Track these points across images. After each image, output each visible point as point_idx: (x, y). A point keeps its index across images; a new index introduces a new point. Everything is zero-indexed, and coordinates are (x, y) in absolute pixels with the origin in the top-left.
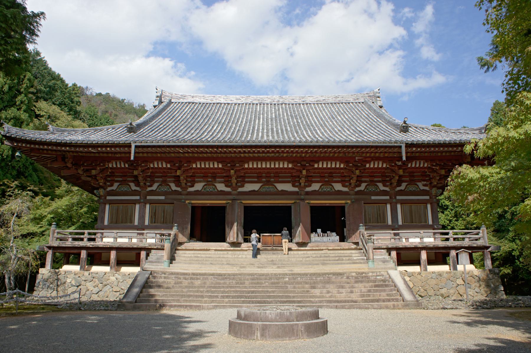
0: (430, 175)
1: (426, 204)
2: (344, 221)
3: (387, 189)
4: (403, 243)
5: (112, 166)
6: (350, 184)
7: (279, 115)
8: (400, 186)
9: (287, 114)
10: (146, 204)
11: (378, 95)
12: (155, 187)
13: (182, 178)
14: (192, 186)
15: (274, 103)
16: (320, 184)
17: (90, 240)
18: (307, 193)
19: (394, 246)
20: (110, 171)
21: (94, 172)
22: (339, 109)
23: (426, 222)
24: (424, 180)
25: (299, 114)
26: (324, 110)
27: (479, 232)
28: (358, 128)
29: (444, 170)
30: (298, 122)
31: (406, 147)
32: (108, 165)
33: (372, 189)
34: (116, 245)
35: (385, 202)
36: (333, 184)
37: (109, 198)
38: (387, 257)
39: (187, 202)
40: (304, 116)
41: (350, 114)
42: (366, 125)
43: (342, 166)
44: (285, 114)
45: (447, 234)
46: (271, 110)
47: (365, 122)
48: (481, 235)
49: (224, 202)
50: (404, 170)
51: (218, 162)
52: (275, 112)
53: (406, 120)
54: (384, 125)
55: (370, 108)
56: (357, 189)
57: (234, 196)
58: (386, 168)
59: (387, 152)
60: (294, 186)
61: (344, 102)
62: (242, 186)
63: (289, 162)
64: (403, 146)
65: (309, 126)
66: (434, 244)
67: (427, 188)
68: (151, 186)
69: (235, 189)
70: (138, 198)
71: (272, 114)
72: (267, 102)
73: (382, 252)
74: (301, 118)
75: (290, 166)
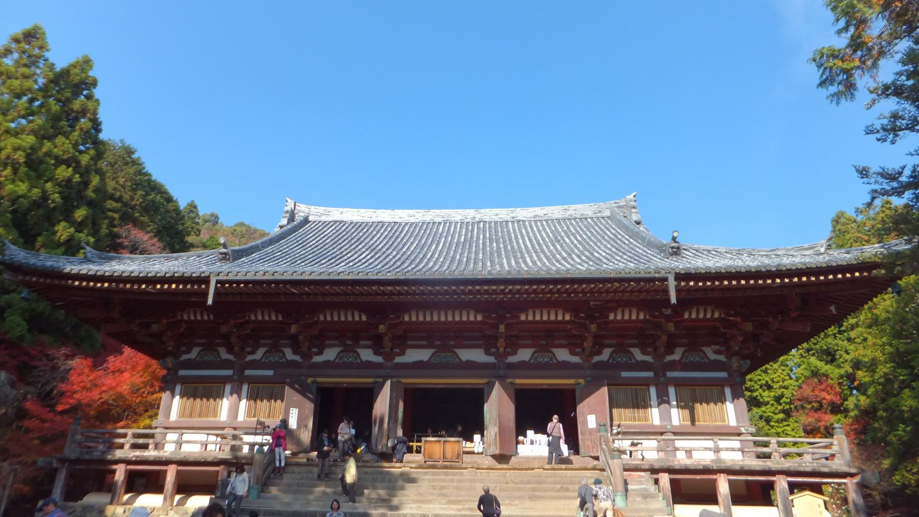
0: (725, 334)
1: (723, 386)
2: (575, 417)
3: (649, 358)
4: (681, 459)
5: (189, 317)
6: (583, 349)
7: (472, 236)
8: (672, 353)
9: (484, 237)
10: (242, 383)
11: (633, 203)
12: (259, 355)
13: (301, 338)
14: (320, 353)
15: (467, 220)
16: (533, 350)
17: (135, 446)
18: (511, 366)
19: (665, 465)
20: (184, 325)
21: (155, 327)
22: (568, 228)
23: (723, 420)
24: (716, 344)
25: (503, 236)
26: (544, 230)
27: (832, 444)
28: (596, 254)
29: (750, 324)
30: (498, 247)
31: (676, 279)
32: (182, 316)
33: (621, 359)
34: (179, 457)
35: (646, 383)
36: (554, 350)
37: (182, 373)
38: (652, 488)
39: (309, 380)
40: (510, 240)
41: (587, 235)
42: (610, 249)
43: (567, 317)
44: (481, 236)
45: (766, 445)
46: (460, 231)
47: (609, 246)
48: (835, 448)
49: (371, 380)
50: (676, 325)
51: (360, 312)
52: (466, 234)
53: (676, 234)
54: (640, 249)
55: (620, 225)
56: (596, 359)
57: (388, 371)
58: (644, 321)
59: (643, 291)
60: (488, 353)
61: (577, 216)
62: (402, 353)
63: (477, 311)
64: (672, 284)
65: (513, 253)
66: (741, 463)
67: (722, 358)
68: (253, 352)
69: (389, 357)
70: (229, 372)
71: (460, 236)
72: (456, 219)
73: (642, 477)
74: (504, 242)
75: (479, 318)
